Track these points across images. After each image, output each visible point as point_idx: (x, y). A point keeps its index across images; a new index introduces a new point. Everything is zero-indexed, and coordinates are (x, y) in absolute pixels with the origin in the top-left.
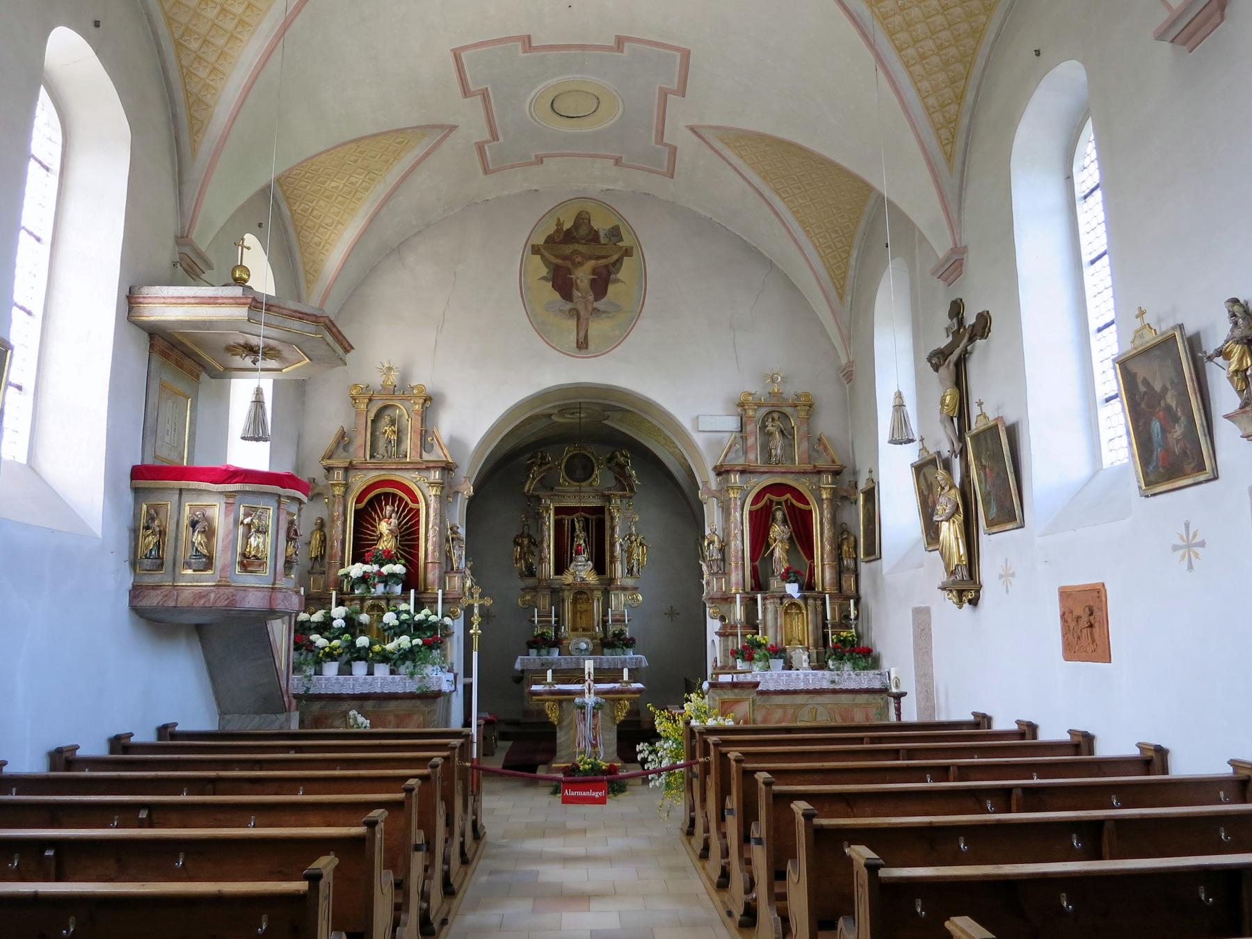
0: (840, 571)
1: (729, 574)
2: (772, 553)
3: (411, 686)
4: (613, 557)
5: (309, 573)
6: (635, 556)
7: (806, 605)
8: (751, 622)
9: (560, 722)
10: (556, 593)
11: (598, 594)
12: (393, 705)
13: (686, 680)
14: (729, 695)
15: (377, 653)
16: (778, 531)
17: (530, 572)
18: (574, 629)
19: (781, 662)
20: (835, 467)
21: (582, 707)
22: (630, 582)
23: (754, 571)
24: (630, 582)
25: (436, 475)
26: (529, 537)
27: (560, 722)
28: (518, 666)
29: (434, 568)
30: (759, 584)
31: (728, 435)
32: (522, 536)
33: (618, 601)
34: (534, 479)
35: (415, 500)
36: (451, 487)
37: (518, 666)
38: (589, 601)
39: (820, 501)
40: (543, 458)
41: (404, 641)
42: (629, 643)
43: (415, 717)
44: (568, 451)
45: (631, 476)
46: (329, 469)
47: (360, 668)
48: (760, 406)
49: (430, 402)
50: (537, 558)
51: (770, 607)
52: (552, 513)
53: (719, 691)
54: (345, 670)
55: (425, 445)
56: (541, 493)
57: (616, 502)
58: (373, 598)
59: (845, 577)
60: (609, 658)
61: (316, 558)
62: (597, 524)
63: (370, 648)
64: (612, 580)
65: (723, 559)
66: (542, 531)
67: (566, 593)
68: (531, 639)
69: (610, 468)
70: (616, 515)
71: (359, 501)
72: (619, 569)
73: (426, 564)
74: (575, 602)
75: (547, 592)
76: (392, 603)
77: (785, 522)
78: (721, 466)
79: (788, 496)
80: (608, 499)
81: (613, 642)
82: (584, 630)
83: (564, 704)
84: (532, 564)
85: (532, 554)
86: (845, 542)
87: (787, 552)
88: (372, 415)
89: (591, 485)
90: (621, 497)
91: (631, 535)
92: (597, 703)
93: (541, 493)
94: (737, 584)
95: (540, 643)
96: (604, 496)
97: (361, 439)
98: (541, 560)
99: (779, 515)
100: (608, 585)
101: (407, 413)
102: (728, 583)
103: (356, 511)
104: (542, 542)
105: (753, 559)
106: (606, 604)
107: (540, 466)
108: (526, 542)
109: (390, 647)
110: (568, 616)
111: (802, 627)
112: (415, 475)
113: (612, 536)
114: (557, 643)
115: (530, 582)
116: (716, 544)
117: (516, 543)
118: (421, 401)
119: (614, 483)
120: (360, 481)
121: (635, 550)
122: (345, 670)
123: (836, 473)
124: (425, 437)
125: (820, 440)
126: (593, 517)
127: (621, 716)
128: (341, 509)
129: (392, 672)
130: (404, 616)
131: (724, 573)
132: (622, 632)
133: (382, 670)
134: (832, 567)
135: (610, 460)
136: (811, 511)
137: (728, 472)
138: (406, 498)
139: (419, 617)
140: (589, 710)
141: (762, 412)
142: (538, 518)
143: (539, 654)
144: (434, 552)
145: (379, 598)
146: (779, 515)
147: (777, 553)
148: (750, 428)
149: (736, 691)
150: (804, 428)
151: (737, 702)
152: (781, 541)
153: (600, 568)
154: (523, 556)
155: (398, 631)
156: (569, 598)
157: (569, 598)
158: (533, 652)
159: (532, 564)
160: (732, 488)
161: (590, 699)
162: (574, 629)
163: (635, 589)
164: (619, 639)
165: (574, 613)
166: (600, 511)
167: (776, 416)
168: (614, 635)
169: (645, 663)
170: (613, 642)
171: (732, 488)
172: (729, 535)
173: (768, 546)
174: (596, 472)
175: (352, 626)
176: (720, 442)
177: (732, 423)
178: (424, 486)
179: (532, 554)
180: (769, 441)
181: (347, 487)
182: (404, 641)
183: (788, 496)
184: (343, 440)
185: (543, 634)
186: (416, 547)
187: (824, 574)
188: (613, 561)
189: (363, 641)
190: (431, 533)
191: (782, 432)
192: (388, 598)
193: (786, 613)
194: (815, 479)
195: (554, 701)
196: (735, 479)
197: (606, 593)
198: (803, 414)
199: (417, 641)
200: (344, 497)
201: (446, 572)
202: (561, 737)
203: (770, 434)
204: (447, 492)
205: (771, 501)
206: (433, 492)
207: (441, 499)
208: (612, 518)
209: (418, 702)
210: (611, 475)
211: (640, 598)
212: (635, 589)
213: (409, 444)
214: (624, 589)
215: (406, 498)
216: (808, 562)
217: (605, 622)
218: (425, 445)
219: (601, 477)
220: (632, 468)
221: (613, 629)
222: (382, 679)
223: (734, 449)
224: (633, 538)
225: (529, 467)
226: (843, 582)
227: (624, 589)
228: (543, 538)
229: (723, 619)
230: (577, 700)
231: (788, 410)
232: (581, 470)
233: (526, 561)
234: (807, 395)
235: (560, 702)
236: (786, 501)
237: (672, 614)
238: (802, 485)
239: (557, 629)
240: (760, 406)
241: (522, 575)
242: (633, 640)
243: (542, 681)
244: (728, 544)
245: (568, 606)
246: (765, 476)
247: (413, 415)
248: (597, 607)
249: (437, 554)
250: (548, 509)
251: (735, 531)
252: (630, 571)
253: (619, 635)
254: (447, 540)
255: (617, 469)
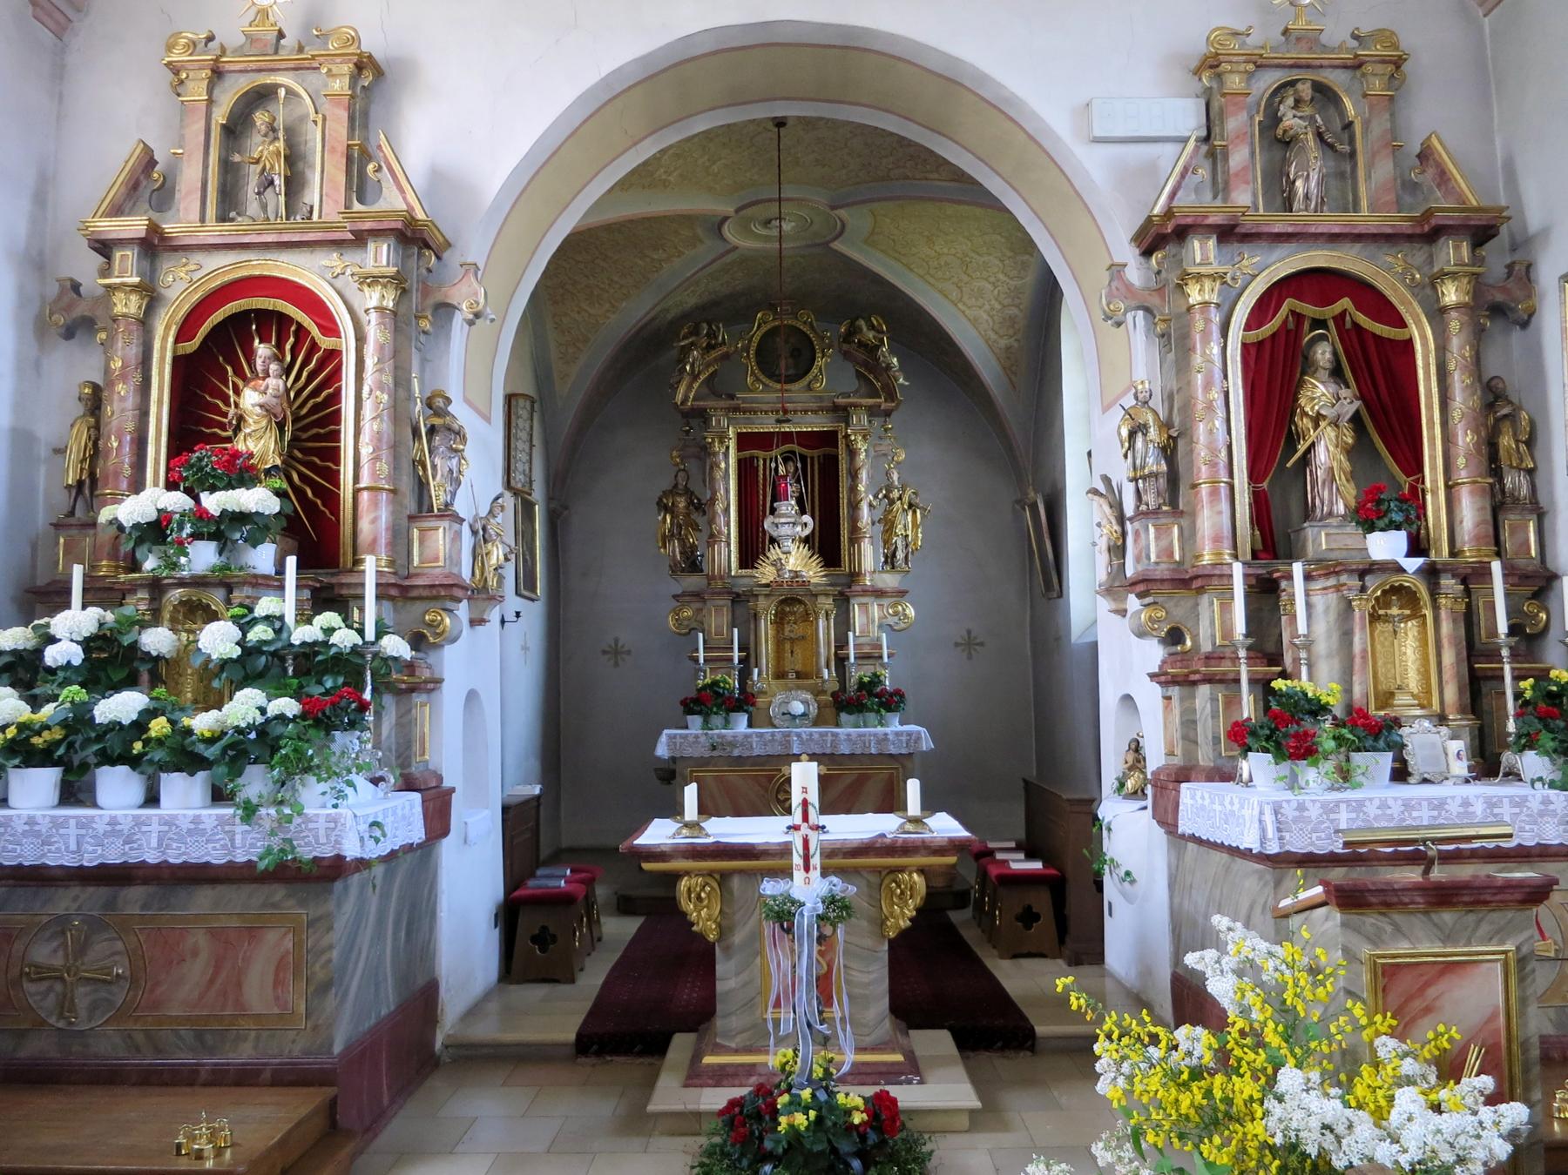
0: (1499, 505)
1: (1193, 515)
2: (1306, 460)
3: (243, 844)
4: (855, 529)
5: (58, 526)
6: (899, 530)
7: (1434, 592)
8: (1267, 646)
9: (724, 931)
10: (740, 600)
11: (826, 603)
12: (203, 900)
13: (1025, 781)
14: (1416, 942)
15: (160, 742)
16: (1323, 397)
17: (692, 564)
18: (780, 675)
19: (1386, 760)
20: (1477, 220)
21: (784, 915)
22: (889, 581)
23: (1260, 504)
24: (889, 581)
25: (379, 257)
26: (689, 493)
27: (724, 931)
28: (662, 750)
29: (375, 504)
30: (1273, 537)
31: (1171, 149)
32: (673, 491)
33: (867, 618)
34: (695, 377)
35: (331, 329)
36: (426, 291)
37: (662, 750)
38: (808, 617)
39: (1438, 314)
40: (712, 335)
41: (245, 706)
42: (891, 702)
43: (271, 936)
44: (763, 323)
45: (889, 367)
46: (104, 247)
47: (117, 788)
48: (1261, 64)
49: (371, 79)
50: (705, 536)
51: (1319, 601)
52: (732, 444)
53: (1370, 920)
54: (75, 792)
55: (359, 185)
56: (708, 404)
57: (859, 420)
58: (182, 583)
59: (1509, 521)
60: (850, 734)
61: (80, 483)
62: (824, 477)
63: (140, 726)
64: (855, 576)
65: (1173, 479)
66: (712, 479)
67: (762, 603)
68: (693, 694)
69: (847, 355)
70: (862, 446)
71: (184, 334)
72: (869, 556)
73: (356, 492)
74: (780, 620)
75: (725, 602)
76: (237, 595)
77: (1336, 373)
78: (1169, 213)
79: (1345, 303)
80: (842, 412)
81: (861, 698)
82: (799, 675)
83: (736, 882)
84: (694, 548)
85: (696, 528)
86: (1506, 427)
87: (1350, 452)
88: (220, 116)
89: (809, 388)
90: (873, 412)
91: (889, 489)
92: (831, 901)
93: (708, 404)
94: (1217, 539)
95: (709, 702)
96: (835, 408)
97: (194, 175)
98: (713, 539)
99: (1322, 354)
100: (846, 588)
101: (315, 105)
102: (1188, 537)
103: (177, 360)
104: (713, 500)
105: (1254, 475)
106: (844, 623)
107: (710, 347)
108: (682, 503)
109: (203, 723)
110: (766, 648)
111: (1414, 658)
112: (332, 259)
113: (853, 489)
114: (743, 701)
115: (693, 582)
116: (1153, 433)
117: (663, 507)
118: (347, 68)
119: (852, 383)
120: (183, 283)
121: (900, 517)
122: (75, 792)
123: (1482, 233)
124: (359, 170)
125: (1425, 155)
126: (815, 453)
127: (902, 916)
128: (134, 351)
129: (219, 796)
130: (260, 633)
131: (1176, 512)
132: (876, 679)
133: (184, 794)
134: (1477, 491)
135: (848, 338)
136: (1409, 343)
137: (1182, 234)
138: (307, 322)
139: (302, 634)
140: (805, 920)
141: (1269, 80)
142: (704, 454)
143: (706, 725)
144: (375, 459)
145: (199, 582)
146: (1322, 354)
147: (1322, 455)
148: (1235, 123)
149: (1447, 917)
150: (1380, 126)
151: (1450, 968)
152: (1335, 424)
153: (828, 544)
154: (676, 533)
155: (220, 680)
156: (767, 610)
157: (767, 610)
158: (695, 721)
159: (694, 548)
160: (1199, 277)
161: (808, 888)
162: (780, 675)
163: (901, 593)
164: (871, 694)
165: (779, 642)
166: (827, 439)
167: (1305, 90)
168: (861, 685)
169: (927, 744)
170: (861, 698)
171: (1199, 277)
172: (1188, 407)
173: (1292, 440)
174: (819, 362)
175: (110, 661)
176: (1150, 169)
177: (1185, 117)
178: (350, 285)
179: (696, 528)
180: (1285, 162)
181: (151, 295)
182: (245, 706)
183: (1345, 303)
184: (146, 182)
185: (715, 683)
186: (334, 455)
187: (1457, 512)
188: (855, 539)
189: (122, 706)
190: (368, 411)
191: (1319, 136)
192: (224, 580)
193: (1374, 618)
194: (1419, 254)
195: (710, 874)
196: (1202, 251)
197: (843, 601)
198: (1377, 86)
199: (288, 706)
200: (145, 323)
201: (411, 518)
202: (728, 976)
203: (1287, 143)
204: (419, 310)
205: (1298, 317)
206: (373, 297)
207: (397, 320)
208: (852, 453)
209: (279, 892)
210: (849, 370)
211: (911, 612)
212: (901, 593)
213: (324, 192)
214: (879, 593)
215: (307, 322)
216: (1405, 482)
217: (841, 661)
218: (359, 185)
219: (829, 375)
220: (892, 352)
221: (858, 673)
222: (181, 821)
223: (1191, 180)
224: (895, 494)
225: (686, 351)
226: (1506, 535)
227: (879, 593)
228: (714, 493)
229: (1174, 637)
230: (769, 887)
231: (1336, 79)
232: (787, 358)
233: (683, 542)
234: (1385, 36)
235: (724, 878)
236: (1340, 318)
237: (969, 644)
238: (1384, 272)
239: (745, 675)
240: (1261, 64)
241: (675, 569)
242: (898, 693)
243: (673, 809)
244: (1187, 432)
245: (766, 629)
246: (1282, 250)
247: (326, 107)
248: (824, 629)
249: (384, 467)
250: (722, 438)
251: (1204, 392)
252: (890, 559)
253: (870, 687)
254: (416, 432)
255: (861, 355)
